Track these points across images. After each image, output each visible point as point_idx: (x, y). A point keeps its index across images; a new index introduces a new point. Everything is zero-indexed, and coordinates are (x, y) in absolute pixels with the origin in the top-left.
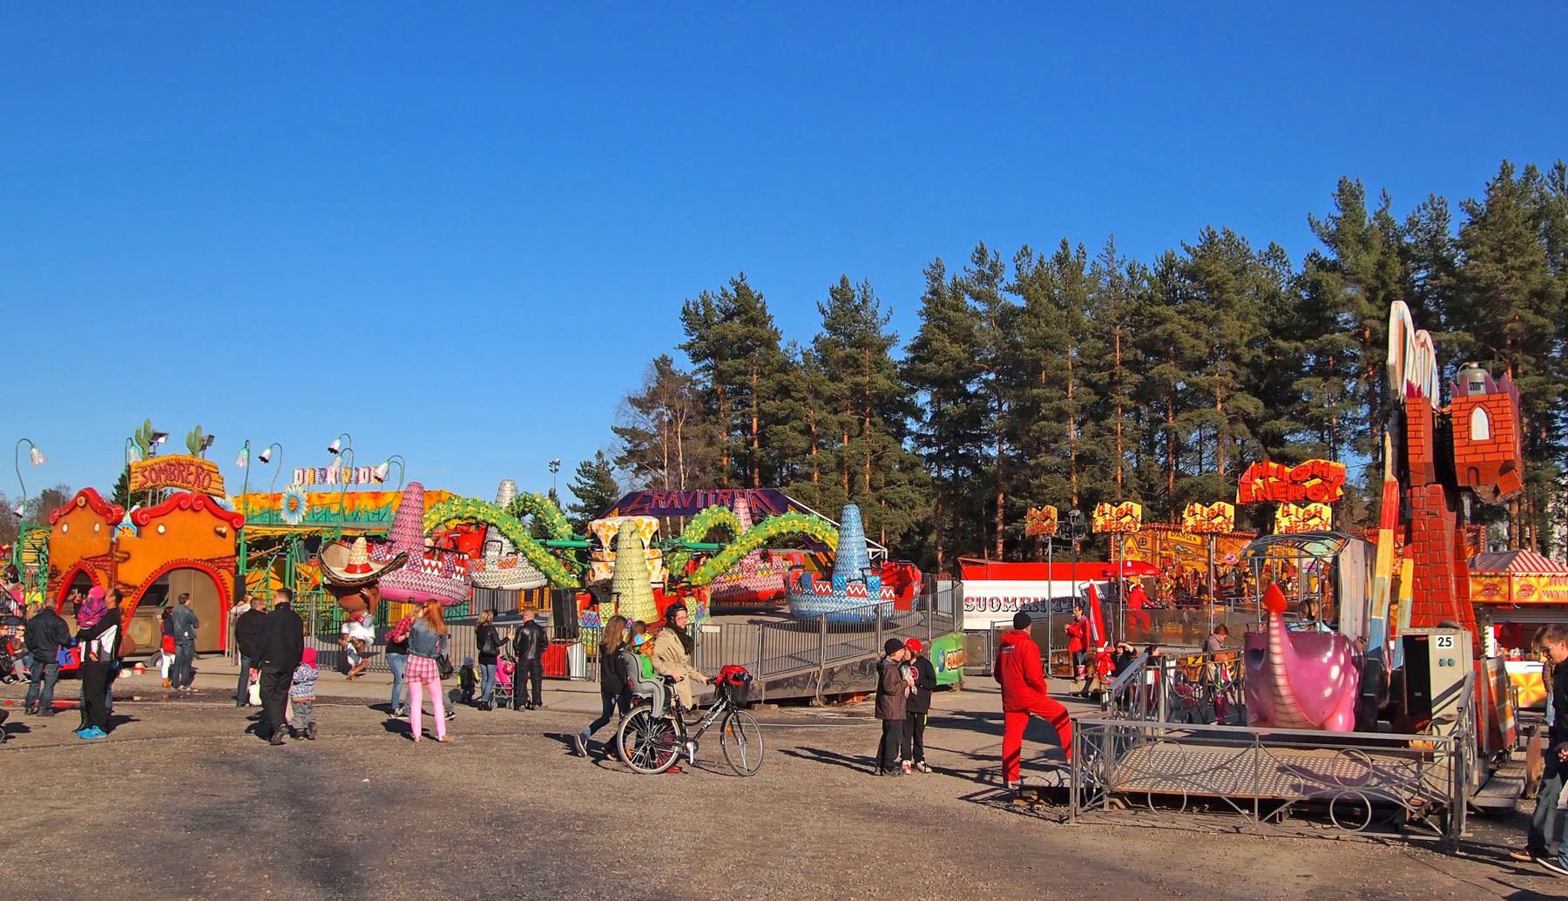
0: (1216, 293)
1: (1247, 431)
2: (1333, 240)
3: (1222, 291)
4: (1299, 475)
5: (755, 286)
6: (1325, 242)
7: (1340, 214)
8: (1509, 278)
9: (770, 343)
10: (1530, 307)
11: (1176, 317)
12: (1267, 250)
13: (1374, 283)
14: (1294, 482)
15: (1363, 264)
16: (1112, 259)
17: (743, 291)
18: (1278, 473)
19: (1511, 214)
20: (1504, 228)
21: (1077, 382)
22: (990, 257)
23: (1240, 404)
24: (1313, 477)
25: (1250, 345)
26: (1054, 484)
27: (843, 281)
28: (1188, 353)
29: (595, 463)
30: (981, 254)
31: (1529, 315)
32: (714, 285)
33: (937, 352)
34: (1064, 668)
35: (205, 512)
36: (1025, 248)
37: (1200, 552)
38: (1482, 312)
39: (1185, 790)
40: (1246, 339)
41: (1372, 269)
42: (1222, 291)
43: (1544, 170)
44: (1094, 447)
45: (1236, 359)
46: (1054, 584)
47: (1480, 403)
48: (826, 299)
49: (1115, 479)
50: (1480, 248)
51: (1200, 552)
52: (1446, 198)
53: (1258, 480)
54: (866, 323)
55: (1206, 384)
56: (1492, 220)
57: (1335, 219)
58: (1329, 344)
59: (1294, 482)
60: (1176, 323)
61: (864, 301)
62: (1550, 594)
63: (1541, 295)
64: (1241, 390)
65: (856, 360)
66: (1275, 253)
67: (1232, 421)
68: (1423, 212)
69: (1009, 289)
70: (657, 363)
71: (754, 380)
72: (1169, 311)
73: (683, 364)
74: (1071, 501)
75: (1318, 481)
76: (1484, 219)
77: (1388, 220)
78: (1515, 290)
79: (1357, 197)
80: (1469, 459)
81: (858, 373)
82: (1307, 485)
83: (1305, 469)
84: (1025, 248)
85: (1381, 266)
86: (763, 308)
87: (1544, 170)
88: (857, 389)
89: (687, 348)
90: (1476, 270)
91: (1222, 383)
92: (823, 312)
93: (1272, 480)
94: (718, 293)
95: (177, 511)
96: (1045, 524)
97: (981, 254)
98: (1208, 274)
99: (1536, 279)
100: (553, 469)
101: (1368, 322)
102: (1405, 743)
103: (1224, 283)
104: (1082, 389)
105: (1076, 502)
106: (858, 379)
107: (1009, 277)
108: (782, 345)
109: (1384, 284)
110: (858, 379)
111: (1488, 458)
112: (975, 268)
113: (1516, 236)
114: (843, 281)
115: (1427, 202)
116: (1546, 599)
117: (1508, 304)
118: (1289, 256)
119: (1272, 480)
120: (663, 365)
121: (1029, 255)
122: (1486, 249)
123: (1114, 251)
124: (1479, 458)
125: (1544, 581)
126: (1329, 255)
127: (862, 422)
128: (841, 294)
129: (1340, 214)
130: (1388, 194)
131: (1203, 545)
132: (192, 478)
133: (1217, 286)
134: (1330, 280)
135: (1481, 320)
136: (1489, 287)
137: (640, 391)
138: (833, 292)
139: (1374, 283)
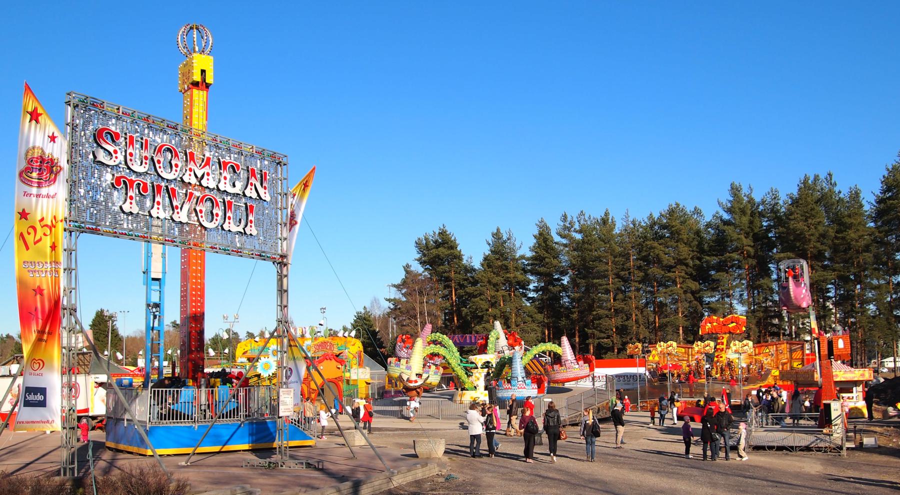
0: (675, 235)
1: (692, 297)
2: (729, 211)
3: (679, 234)
4: (726, 322)
5: (449, 230)
6: (725, 211)
7: (732, 199)
8: (810, 229)
9: (459, 257)
10: (819, 242)
11: (659, 247)
12: (693, 210)
13: (748, 230)
14: (724, 325)
15: (744, 222)
16: (628, 220)
17: (443, 233)
18: (717, 321)
19: (809, 199)
20: (807, 206)
21: (614, 276)
22: (569, 219)
23: (689, 285)
24: (732, 322)
25: (692, 258)
26: (605, 323)
27: (498, 230)
28: (665, 263)
29: (363, 311)
30: (565, 217)
31: (818, 245)
32: (429, 230)
33: (547, 263)
34: (645, 407)
35: (333, 360)
36: (582, 212)
37: (684, 355)
38: (798, 244)
39: (775, 444)
40: (691, 256)
41: (747, 225)
42: (679, 234)
43: (822, 176)
44: (624, 306)
45: (687, 265)
46: (636, 372)
47: (841, 338)
48: (490, 239)
49: (632, 320)
50: (796, 216)
51: (684, 355)
52: (778, 189)
53: (709, 324)
54: (510, 249)
55: (674, 277)
56: (801, 202)
57: (730, 201)
58: (729, 258)
59: (724, 325)
60: (659, 249)
61: (508, 239)
62: (844, 378)
63: (823, 236)
64: (688, 278)
65: (505, 266)
66: (697, 211)
67: (685, 292)
68: (768, 196)
69: (576, 232)
70: (404, 267)
71: (453, 275)
72: (656, 244)
73: (418, 268)
74: (612, 330)
75: (734, 324)
76: (797, 202)
77: (752, 199)
78: (812, 235)
79: (739, 191)
80: (838, 353)
81: (507, 272)
82: (730, 326)
83: (729, 319)
84: (582, 212)
85: (751, 222)
86: (455, 240)
87: (822, 176)
88: (507, 281)
89: (418, 260)
90: (795, 225)
91: (680, 277)
92: (489, 244)
93: (715, 324)
94: (432, 233)
95: (326, 361)
96: (636, 350)
97: (565, 217)
98: (673, 227)
99: (821, 229)
100: (322, 311)
101: (745, 248)
102: (822, 431)
103: (680, 231)
104: (616, 280)
105: (614, 330)
106: (508, 275)
107: (577, 226)
108: (465, 258)
109: (752, 230)
110: (508, 275)
111: (843, 353)
112: (562, 224)
113: (812, 209)
114: (498, 230)
115: (770, 191)
116: (843, 379)
117: (810, 240)
118: (703, 212)
119: (715, 324)
120: (407, 268)
121: (584, 215)
122: (799, 215)
123: (629, 217)
124: (841, 353)
125: (842, 373)
126: (726, 217)
127: (510, 295)
128: (497, 235)
129: (732, 199)
130: (752, 187)
131: (685, 352)
132: (328, 347)
133: (677, 232)
134: (729, 230)
135: (798, 247)
136: (801, 233)
137: (398, 281)
138: (493, 235)
139: (748, 230)
